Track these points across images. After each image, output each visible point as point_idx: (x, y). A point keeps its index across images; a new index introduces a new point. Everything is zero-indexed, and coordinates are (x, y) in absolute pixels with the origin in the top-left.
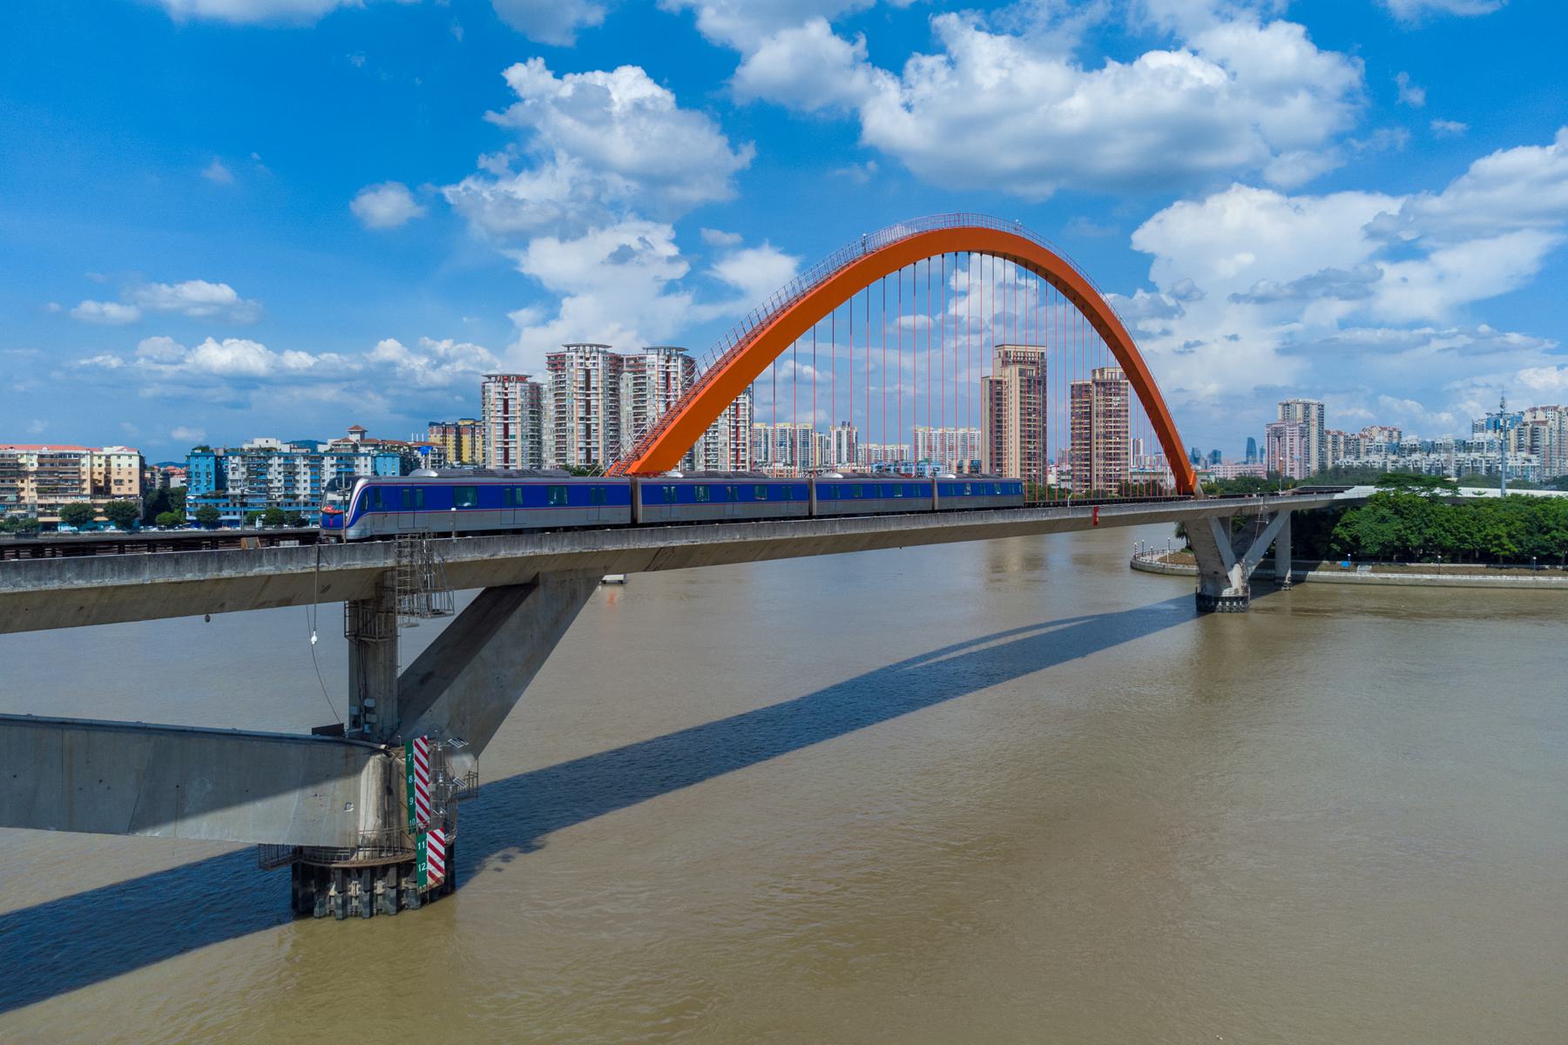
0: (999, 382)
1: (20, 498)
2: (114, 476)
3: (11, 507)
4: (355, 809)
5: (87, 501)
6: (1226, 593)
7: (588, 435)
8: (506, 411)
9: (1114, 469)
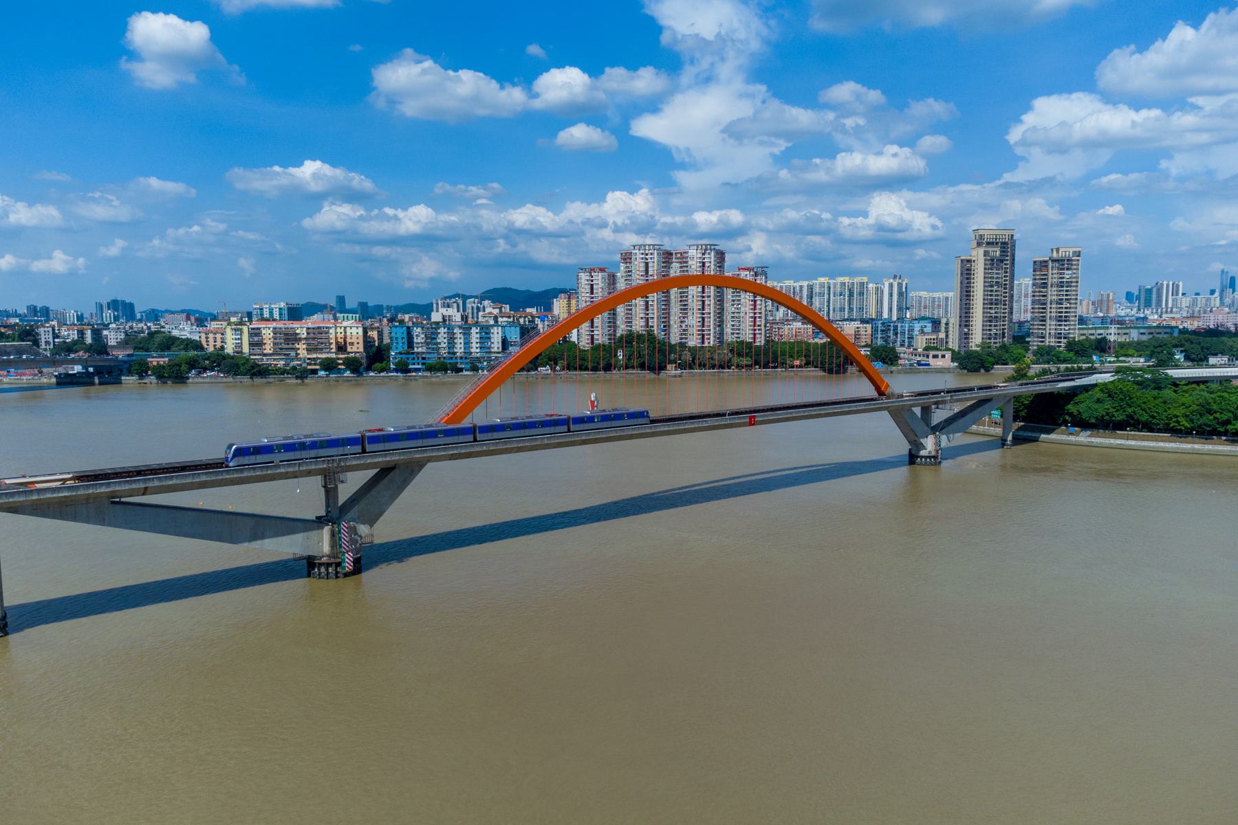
0: (969, 261)
1: (297, 354)
2: (349, 340)
3: (292, 360)
4: (321, 543)
5: (334, 356)
6: (923, 453)
7: (647, 309)
8: (592, 292)
9: (1064, 329)
